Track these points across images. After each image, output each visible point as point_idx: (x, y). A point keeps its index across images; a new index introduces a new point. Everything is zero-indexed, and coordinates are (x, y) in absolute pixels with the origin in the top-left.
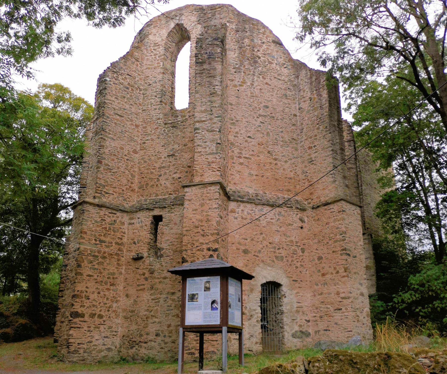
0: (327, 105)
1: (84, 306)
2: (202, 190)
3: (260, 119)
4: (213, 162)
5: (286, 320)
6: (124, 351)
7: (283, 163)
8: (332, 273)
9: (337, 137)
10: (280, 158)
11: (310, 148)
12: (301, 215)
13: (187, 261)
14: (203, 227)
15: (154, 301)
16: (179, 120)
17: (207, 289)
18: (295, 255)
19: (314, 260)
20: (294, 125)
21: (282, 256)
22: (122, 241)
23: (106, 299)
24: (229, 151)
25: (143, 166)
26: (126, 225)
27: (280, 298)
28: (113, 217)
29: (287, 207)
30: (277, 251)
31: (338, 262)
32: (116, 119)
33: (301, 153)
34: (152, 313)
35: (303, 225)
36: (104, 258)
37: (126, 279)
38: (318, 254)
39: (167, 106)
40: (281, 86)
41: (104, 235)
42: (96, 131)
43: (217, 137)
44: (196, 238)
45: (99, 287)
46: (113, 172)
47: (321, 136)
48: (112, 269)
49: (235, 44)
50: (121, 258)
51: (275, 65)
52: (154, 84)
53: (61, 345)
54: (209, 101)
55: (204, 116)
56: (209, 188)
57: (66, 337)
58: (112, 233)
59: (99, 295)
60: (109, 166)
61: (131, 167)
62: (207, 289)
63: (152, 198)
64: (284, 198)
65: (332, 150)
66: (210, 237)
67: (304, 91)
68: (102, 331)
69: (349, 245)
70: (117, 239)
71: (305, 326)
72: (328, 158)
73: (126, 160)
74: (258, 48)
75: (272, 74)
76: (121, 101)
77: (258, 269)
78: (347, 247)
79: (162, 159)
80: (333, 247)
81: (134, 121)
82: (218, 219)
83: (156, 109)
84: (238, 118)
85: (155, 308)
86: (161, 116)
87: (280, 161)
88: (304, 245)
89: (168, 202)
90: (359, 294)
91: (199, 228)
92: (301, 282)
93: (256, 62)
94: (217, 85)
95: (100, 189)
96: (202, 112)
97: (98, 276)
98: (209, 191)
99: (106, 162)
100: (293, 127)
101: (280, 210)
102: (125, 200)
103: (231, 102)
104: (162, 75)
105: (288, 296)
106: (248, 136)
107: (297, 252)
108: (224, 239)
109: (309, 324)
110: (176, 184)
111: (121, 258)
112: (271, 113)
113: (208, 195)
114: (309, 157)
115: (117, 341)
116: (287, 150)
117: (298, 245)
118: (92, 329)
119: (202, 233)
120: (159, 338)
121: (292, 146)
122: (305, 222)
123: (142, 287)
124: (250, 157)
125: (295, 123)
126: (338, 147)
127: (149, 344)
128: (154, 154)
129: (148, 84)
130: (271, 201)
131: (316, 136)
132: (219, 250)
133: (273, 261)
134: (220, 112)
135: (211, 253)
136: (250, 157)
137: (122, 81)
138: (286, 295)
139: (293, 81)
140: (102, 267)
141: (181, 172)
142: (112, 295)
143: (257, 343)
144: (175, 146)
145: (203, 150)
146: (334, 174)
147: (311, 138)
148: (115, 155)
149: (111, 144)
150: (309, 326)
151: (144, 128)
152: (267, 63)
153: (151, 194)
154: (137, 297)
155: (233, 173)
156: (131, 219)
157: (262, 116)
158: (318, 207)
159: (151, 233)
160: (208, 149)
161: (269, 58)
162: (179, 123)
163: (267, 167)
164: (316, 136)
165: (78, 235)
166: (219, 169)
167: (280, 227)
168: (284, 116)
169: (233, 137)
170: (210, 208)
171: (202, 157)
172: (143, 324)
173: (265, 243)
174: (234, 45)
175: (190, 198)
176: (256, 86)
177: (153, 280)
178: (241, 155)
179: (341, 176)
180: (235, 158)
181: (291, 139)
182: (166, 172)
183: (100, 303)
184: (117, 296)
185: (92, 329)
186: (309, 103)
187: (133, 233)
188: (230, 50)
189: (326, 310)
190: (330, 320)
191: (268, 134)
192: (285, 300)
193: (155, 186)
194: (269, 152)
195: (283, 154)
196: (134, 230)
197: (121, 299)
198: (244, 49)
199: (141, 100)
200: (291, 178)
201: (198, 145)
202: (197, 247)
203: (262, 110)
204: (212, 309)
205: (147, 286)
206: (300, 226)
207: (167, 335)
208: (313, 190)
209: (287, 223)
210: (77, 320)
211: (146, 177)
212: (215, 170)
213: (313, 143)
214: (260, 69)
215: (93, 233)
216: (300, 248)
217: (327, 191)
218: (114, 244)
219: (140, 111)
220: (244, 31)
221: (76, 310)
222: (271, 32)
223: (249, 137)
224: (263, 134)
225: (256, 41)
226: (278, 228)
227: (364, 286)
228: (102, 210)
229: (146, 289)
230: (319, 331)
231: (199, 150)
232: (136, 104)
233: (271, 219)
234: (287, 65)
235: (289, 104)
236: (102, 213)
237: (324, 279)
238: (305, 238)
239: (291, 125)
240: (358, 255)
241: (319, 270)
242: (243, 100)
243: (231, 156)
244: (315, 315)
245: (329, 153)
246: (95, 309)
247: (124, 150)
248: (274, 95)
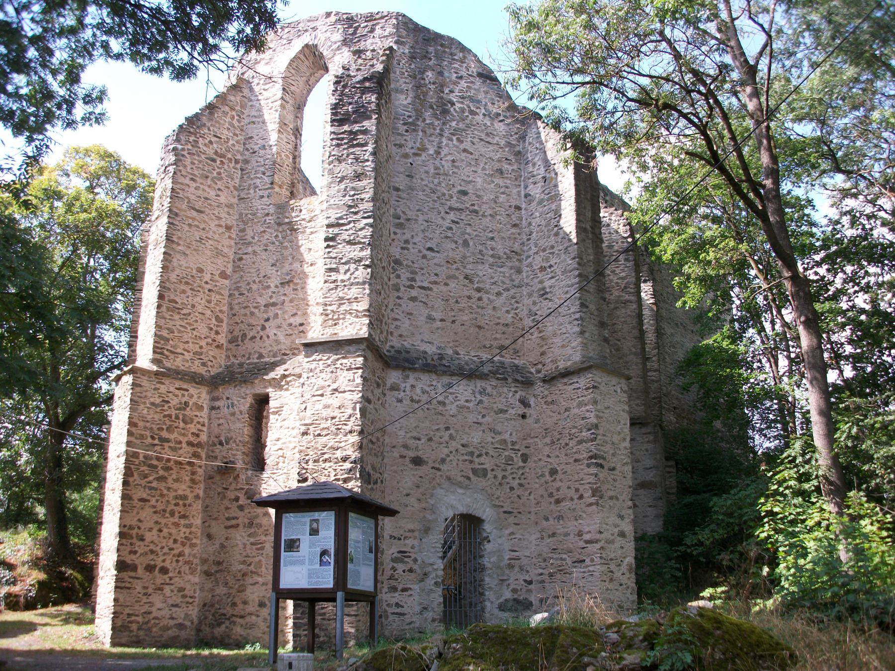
1: (135, 552)
3: (452, 216)
5: (489, 581)
6: (206, 630)
8: (572, 499)
9: (590, 251)
10: (488, 286)
11: (543, 269)
12: (524, 394)
15: (254, 547)
18: (510, 467)
19: (543, 475)
20: (515, 225)
23: (171, 541)
24: (392, 276)
25: (236, 301)
27: (480, 543)
29: (498, 379)
30: (477, 460)
31: (582, 480)
32: (191, 218)
33: (527, 277)
34: (252, 568)
35: (525, 411)
36: (167, 469)
37: (207, 507)
38: (551, 464)
39: (284, 190)
40: (492, 155)
41: (167, 429)
45: (159, 520)
47: (561, 248)
48: (182, 488)
49: (407, 81)
51: (481, 116)
52: (261, 151)
58: (182, 425)
59: (162, 534)
60: (177, 303)
61: (216, 304)
67: (534, 165)
69: (602, 448)
71: (524, 590)
74: (451, 87)
75: (476, 132)
76: (202, 184)
77: (439, 492)
80: (576, 453)
83: (262, 197)
84: (411, 214)
85: (257, 559)
86: (272, 209)
87: (487, 293)
88: (526, 447)
90: (616, 535)
92: (519, 515)
93: (445, 112)
97: (157, 501)
99: (172, 297)
100: (513, 230)
101: (483, 385)
103: (397, 185)
105: (494, 539)
106: (427, 246)
107: (513, 460)
108: (374, 440)
112: (473, 205)
114: (540, 286)
115: (194, 612)
116: (500, 272)
117: (516, 447)
118: (150, 591)
121: (511, 264)
122: (530, 406)
123: (234, 522)
124: (431, 286)
125: (518, 222)
126: (590, 269)
127: (248, 619)
128: (257, 280)
130: (468, 368)
131: (552, 247)
133: (469, 478)
136: (431, 286)
137: (205, 148)
138: (491, 538)
139: (514, 146)
140: (164, 484)
142: (182, 535)
143: (434, 620)
147: (544, 250)
148: (187, 283)
149: (181, 263)
151: (241, 231)
152: (467, 114)
153: (250, 354)
154: (227, 539)
155: (397, 317)
157: (456, 209)
158: (553, 379)
161: (471, 105)
163: (463, 303)
167: (484, 416)
168: (497, 209)
169: (399, 249)
172: (237, 586)
173: (454, 445)
174: (405, 83)
176: (446, 155)
178: (413, 283)
180: (402, 288)
181: (508, 252)
182: (277, 314)
183: (162, 548)
184: (191, 536)
185: (150, 591)
186: (542, 187)
187: (219, 425)
188: (397, 91)
189: (559, 562)
191: (466, 243)
193: (258, 338)
194: (466, 277)
195: (492, 281)
198: (424, 89)
200: (507, 325)
203: (455, 198)
206: (521, 412)
208: (546, 347)
209: (496, 409)
211: (242, 322)
214: (454, 124)
215: (148, 425)
216: (520, 453)
217: (568, 351)
218: (184, 445)
219: (236, 201)
220: (426, 57)
223: (430, 249)
224: (456, 242)
225: (446, 74)
227: (627, 520)
228: (163, 384)
232: (228, 188)
233: (467, 401)
234: (505, 116)
235: (507, 187)
237: (559, 509)
238: (529, 435)
239: (509, 226)
240: (618, 466)
241: (552, 493)
242: (419, 181)
244: (541, 571)
245: (573, 281)
246: (155, 558)
248: (479, 171)
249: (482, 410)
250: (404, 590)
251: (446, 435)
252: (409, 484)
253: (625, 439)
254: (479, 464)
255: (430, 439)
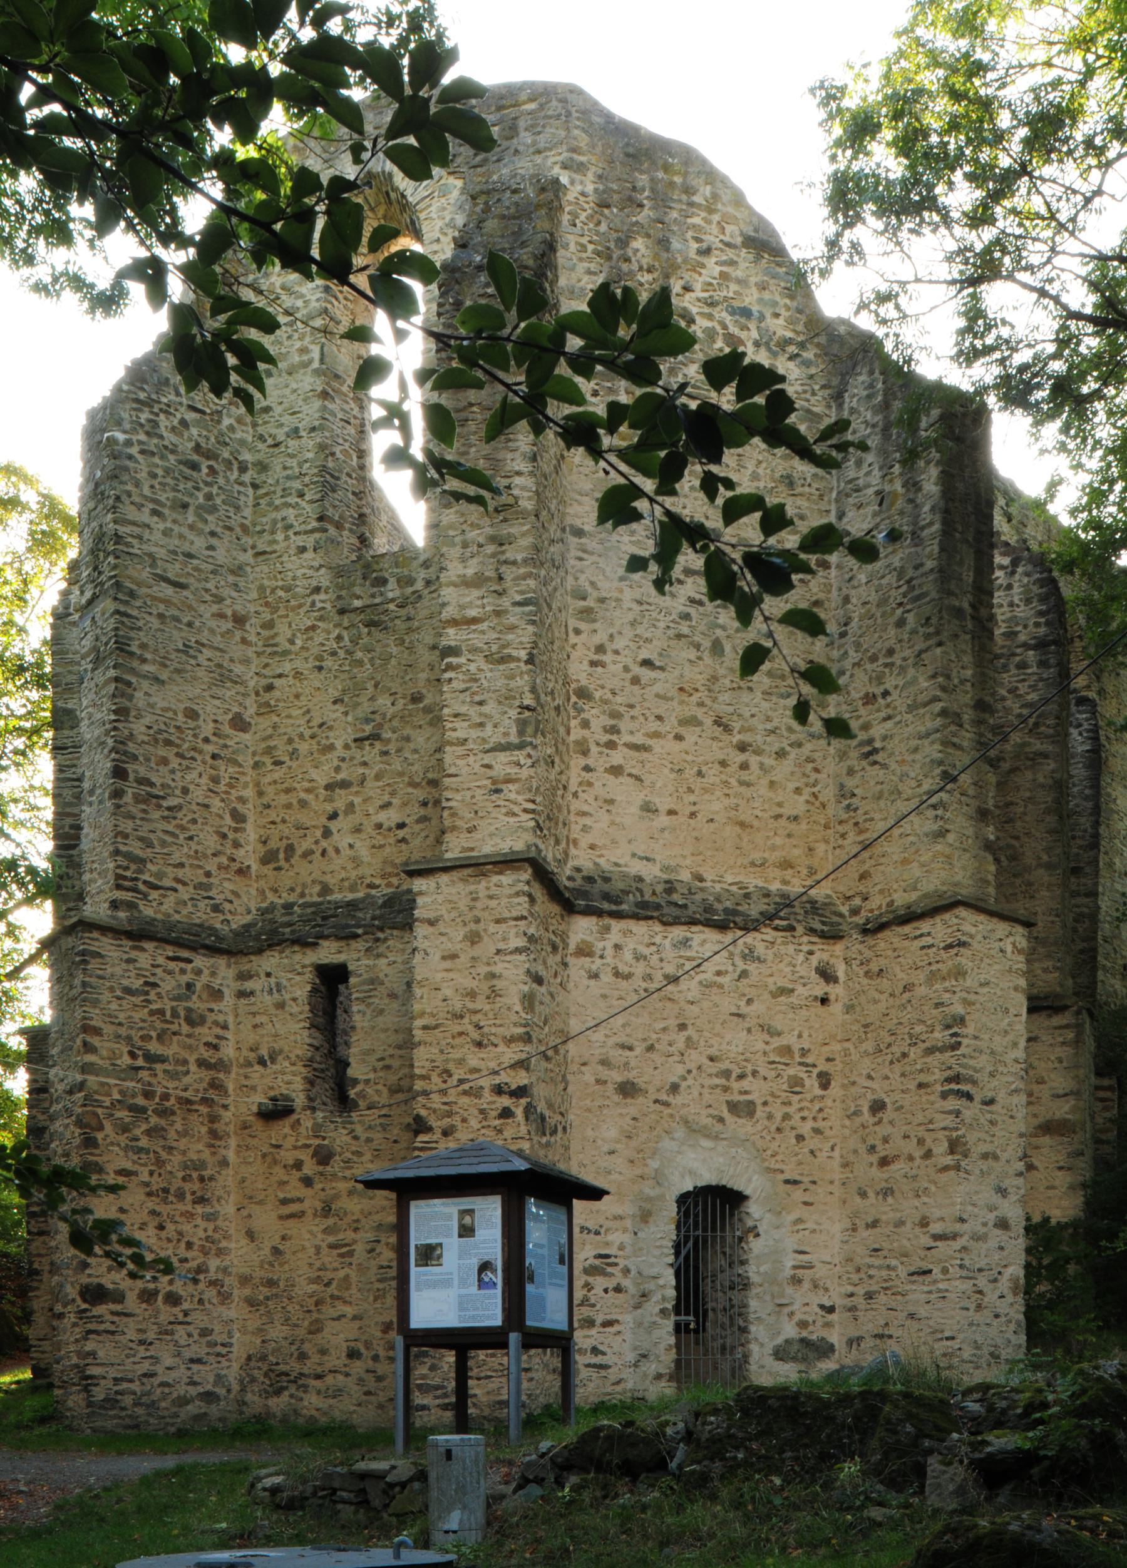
0: (937, 527)
2: (472, 888)
4: (508, 781)
5: (757, 1305)
7: (769, 761)
8: (911, 1158)
9: (967, 659)
13: (429, 1129)
14: (479, 1016)
15: (335, 1252)
16: (390, 595)
17: (466, 1231)
18: (796, 1098)
21: (751, 1103)
22: (220, 1055)
23: (183, 1245)
25: (268, 779)
26: (229, 999)
27: (741, 1239)
28: (183, 971)
29: (776, 929)
30: (736, 1085)
32: (162, 601)
34: (331, 1290)
36: (164, 1113)
38: (873, 1090)
39: (346, 533)
41: (160, 1037)
42: (95, 649)
43: (522, 683)
44: (456, 1055)
45: (158, 1209)
46: (169, 809)
47: (907, 653)
48: (197, 1149)
49: (593, 267)
50: (222, 1112)
53: (64, 1385)
54: (493, 539)
55: (474, 602)
56: (495, 879)
57: (75, 1360)
58: (185, 1029)
59: (163, 1234)
60: (152, 785)
62: (466, 1231)
63: (308, 899)
64: (767, 895)
65: (944, 713)
66: (502, 1048)
68: (182, 1342)
70: (202, 1049)
71: (819, 1324)
72: (926, 742)
73: (208, 758)
76: (175, 521)
78: (962, 1071)
79: (336, 754)
81: (228, 602)
82: (526, 988)
83: (302, 550)
86: (324, 578)
87: (758, 752)
88: (828, 1060)
89: (365, 916)
91: (466, 1020)
92: (812, 1187)
94: (519, 473)
95: (128, 874)
96: (467, 583)
97: (151, 1173)
98: (494, 891)
99: (142, 771)
102: (216, 909)
104: (317, 404)
109: (834, 1317)
110: (388, 850)
111: (222, 1112)
113: (493, 903)
117: (809, 1060)
118: (151, 1336)
119: (475, 1035)
120: (358, 1363)
122: (835, 980)
126: (965, 698)
127: (329, 1380)
128: (307, 733)
129: (270, 441)
131: (891, 652)
132: (535, 1091)
133: (721, 1120)
134: (532, 583)
135: (505, 1101)
136: (649, 742)
137: (174, 439)
138: (761, 1230)
140: (162, 1142)
141: (405, 804)
142: (202, 1234)
143: (659, 1377)
144: (380, 701)
145: (474, 734)
146: (942, 805)
147: (874, 659)
148: (168, 743)
149: (152, 700)
150: (828, 1325)
154: (283, 1238)
155: (586, 808)
156: (243, 976)
159: (312, 1026)
160: (489, 728)
162: (392, 607)
164: (891, 652)
165: (72, 1039)
166: (531, 806)
167: (749, 1002)
170: (498, 952)
171: (471, 759)
173: (695, 1058)
175: (431, 915)
177: (328, 1186)
179: (971, 811)
180: (594, 749)
184: (217, 1236)
187: (255, 1026)
189: (884, 1273)
190: (893, 1305)
192: (756, 1246)
193: (318, 854)
195: (769, 726)
196: (254, 1014)
197: (233, 1245)
199: (247, 512)
200: (796, 818)
201: (456, 716)
202: (461, 1081)
204: (482, 1284)
205: (311, 1200)
206: (819, 993)
207: (382, 1353)
210: (101, 1310)
211: (284, 821)
212: (516, 809)
213: (879, 679)
216: (816, 1071)
218: (193, 1068)
219: (248, 557)
221: (95, 1280)
222: (739, 199)
223: (647, 663)
224: (698, 647)
225: (676, 244)
226: (743, 1003)
227: (1013, 1198)
228: (143, 950)
229: (310, 1212)
230: (859, 1339)
231: (461, 734)
232: (230, 529)
233: (719, 973)
236: (144, 960)
238: (833, 1037)
241: (873, 1147)
243: (577, 743)
244: (850, 1289)
245: (930, 725)
247: (201, 722)
249: (747, 990)
250: (608, 1324)
251: (681, 1038)
252: (613, 1133)
253: (1015, 1044)
254: (741, 1093)
255: (650, 1048)
